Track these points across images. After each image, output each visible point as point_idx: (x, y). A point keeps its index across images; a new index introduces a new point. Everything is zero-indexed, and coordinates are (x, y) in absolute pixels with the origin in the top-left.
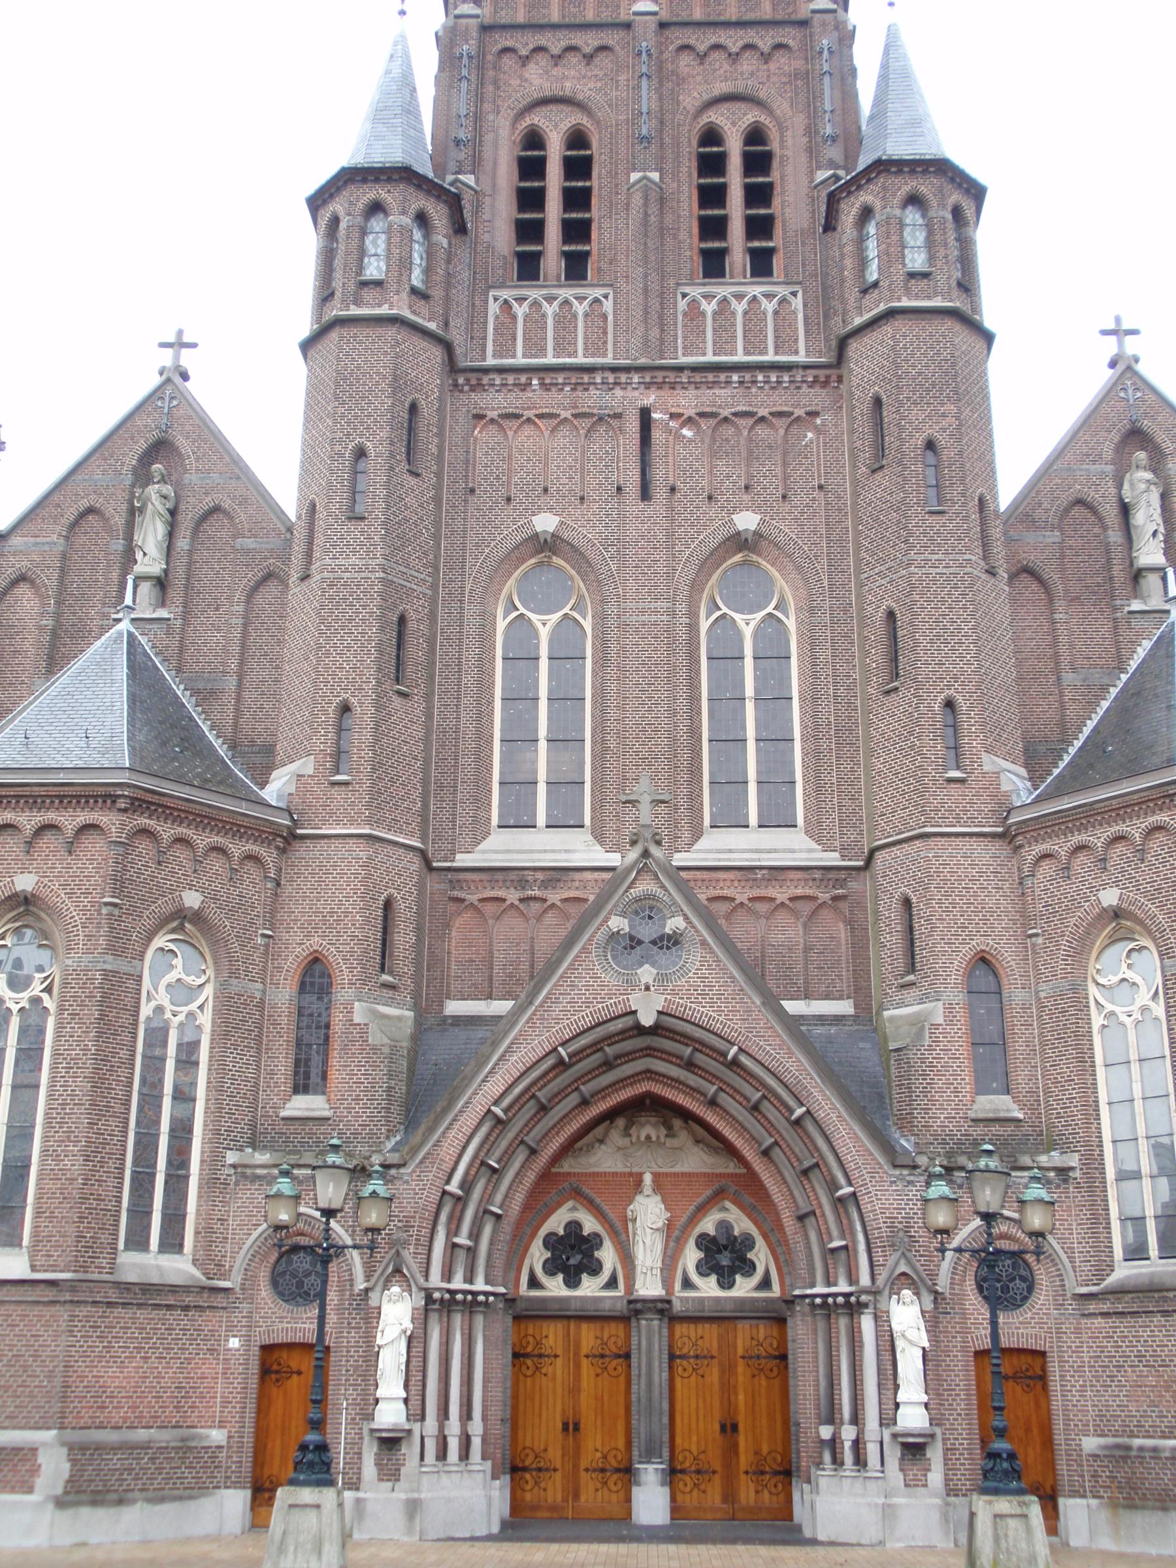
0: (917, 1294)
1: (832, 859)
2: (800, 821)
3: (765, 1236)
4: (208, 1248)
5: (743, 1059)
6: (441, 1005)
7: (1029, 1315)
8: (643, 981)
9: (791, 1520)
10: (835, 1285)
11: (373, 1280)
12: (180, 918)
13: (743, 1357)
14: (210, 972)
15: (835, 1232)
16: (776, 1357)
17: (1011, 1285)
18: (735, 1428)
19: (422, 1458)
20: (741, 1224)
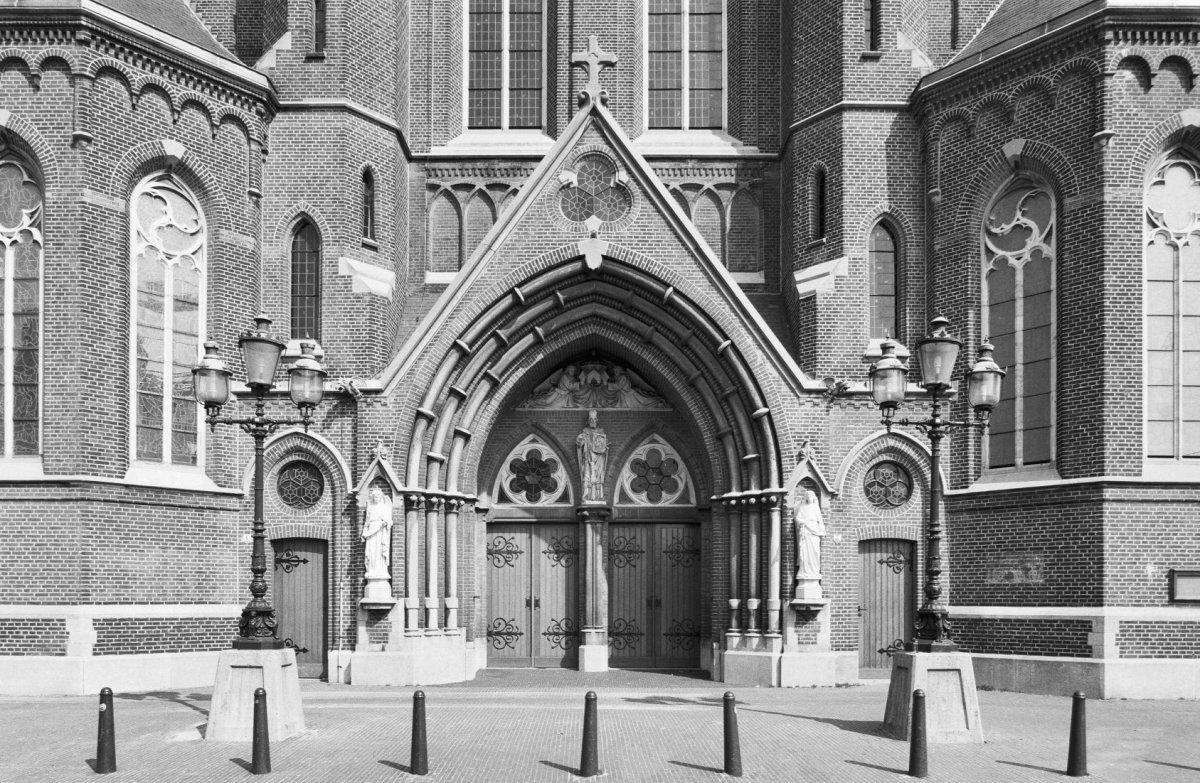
0: (818, 495)
1: (752, 151)
2: (725, 124)
3: (685, 461)
4: (217, 458)
5: (677, 298)
6: (423, 276)
7: (905, 513)
8: (590, 230)
9: (699, 666)
10: (748, 489)
11: (359, 485)
12: (163, 166)
13: (666, 552)
14: (203, 222)
15: (750, 446)
16: (692, 552)
17: (892, 490)
18: (658, 603)
19: (406, 626)
20: (665, 450)
